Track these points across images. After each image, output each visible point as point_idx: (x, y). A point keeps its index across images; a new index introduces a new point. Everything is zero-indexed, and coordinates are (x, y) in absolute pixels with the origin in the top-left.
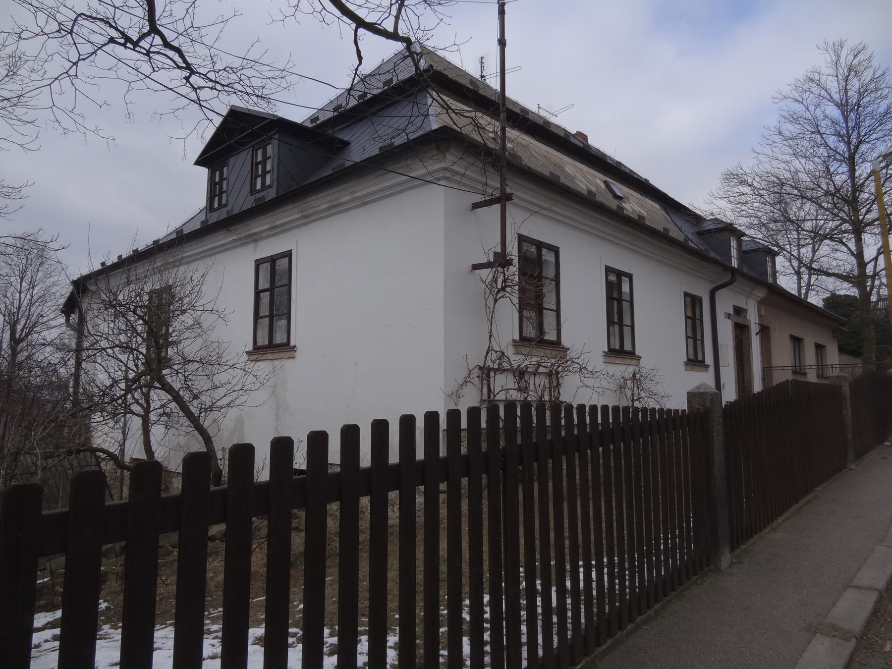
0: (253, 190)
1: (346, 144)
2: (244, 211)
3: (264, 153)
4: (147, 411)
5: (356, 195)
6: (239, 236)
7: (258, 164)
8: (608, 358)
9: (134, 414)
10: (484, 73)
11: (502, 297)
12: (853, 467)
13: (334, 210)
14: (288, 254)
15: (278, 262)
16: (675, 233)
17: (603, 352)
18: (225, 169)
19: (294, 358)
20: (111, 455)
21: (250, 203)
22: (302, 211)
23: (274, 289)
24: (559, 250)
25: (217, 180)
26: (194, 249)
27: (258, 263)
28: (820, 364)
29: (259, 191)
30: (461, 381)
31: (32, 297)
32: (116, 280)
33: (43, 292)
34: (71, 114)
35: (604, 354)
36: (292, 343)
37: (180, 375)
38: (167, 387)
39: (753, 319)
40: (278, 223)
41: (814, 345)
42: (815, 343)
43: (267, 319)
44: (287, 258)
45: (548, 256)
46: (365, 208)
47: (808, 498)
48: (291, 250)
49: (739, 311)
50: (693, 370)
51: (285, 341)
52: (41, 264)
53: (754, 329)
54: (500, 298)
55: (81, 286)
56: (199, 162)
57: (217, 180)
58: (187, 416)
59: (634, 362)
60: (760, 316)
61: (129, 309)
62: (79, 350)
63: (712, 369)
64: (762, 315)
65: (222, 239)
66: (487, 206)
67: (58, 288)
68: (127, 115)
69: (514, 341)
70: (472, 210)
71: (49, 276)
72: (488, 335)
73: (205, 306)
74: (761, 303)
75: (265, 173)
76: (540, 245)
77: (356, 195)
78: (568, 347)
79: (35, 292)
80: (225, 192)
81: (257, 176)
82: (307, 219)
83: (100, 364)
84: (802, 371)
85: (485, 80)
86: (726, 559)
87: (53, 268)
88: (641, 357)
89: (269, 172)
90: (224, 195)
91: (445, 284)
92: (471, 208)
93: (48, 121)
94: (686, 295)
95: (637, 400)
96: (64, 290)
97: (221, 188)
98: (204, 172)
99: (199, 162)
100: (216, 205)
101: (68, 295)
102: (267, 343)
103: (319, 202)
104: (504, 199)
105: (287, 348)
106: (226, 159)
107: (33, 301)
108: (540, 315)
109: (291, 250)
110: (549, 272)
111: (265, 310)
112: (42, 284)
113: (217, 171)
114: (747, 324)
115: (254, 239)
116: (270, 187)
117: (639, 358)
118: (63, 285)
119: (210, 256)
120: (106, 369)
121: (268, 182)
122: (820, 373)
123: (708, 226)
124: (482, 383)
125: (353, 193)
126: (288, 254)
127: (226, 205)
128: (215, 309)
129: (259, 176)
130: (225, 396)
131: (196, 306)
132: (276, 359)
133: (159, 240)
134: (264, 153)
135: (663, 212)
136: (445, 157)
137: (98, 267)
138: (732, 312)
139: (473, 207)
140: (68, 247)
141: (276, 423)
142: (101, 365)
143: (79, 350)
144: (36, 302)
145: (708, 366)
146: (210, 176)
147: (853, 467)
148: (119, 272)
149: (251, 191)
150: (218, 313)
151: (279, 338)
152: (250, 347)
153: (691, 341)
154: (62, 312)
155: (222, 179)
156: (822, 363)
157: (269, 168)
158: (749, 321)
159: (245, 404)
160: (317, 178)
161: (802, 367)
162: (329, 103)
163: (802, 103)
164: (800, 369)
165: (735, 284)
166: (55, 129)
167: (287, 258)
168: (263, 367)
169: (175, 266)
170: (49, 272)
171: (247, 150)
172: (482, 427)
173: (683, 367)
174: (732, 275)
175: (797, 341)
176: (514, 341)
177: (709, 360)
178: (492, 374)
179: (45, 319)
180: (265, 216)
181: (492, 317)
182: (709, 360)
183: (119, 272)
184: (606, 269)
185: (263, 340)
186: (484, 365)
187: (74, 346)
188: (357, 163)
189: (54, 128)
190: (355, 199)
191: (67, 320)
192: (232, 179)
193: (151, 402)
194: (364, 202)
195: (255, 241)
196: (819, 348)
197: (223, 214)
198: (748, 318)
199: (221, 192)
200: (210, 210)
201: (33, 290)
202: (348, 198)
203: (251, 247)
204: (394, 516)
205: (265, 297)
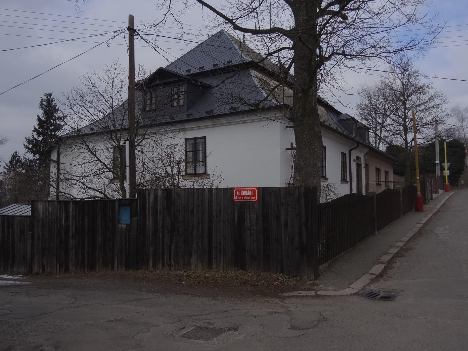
12: (402, 217)
13: (230, 124)
16: (340, 130)
22: (214, 122)
27: (186, 140)
28: (386, 181)
36: (208, 173)
39: (363, 161)
40: (200, 125)
41: (375, 168)
42: (356, 156)
47: (391, 224)
49: (358, 158)
51: (203, 172)
53: (363, 165)
59: (326, 181)
60: (365, 160)
63: (349, 183)
74: (366, 154)
82: (215, 125)
84: (380, 183)
85: (245, 42)
86: (376, 233)
94: (342, 153)
102: (194, 172)
115: (185, 130)
122: (386, 184)
123: (342, 117)
126: (205, 138)
135: (326, 112)
138: (356, 159)
147: (402, 217)
153: (343, 172)
156: (387, 181)
163: (388, 79)
164: (379, 183)
165: (359, 148)
175: (378, 170)
177: (348, 180)
182: (348, 180)
184: (376, 169)
186: (290, 182)
190: (241, 121)
194: (243, 123)
196: (386, 173)
198: (361, 161)
203: (182, 133)
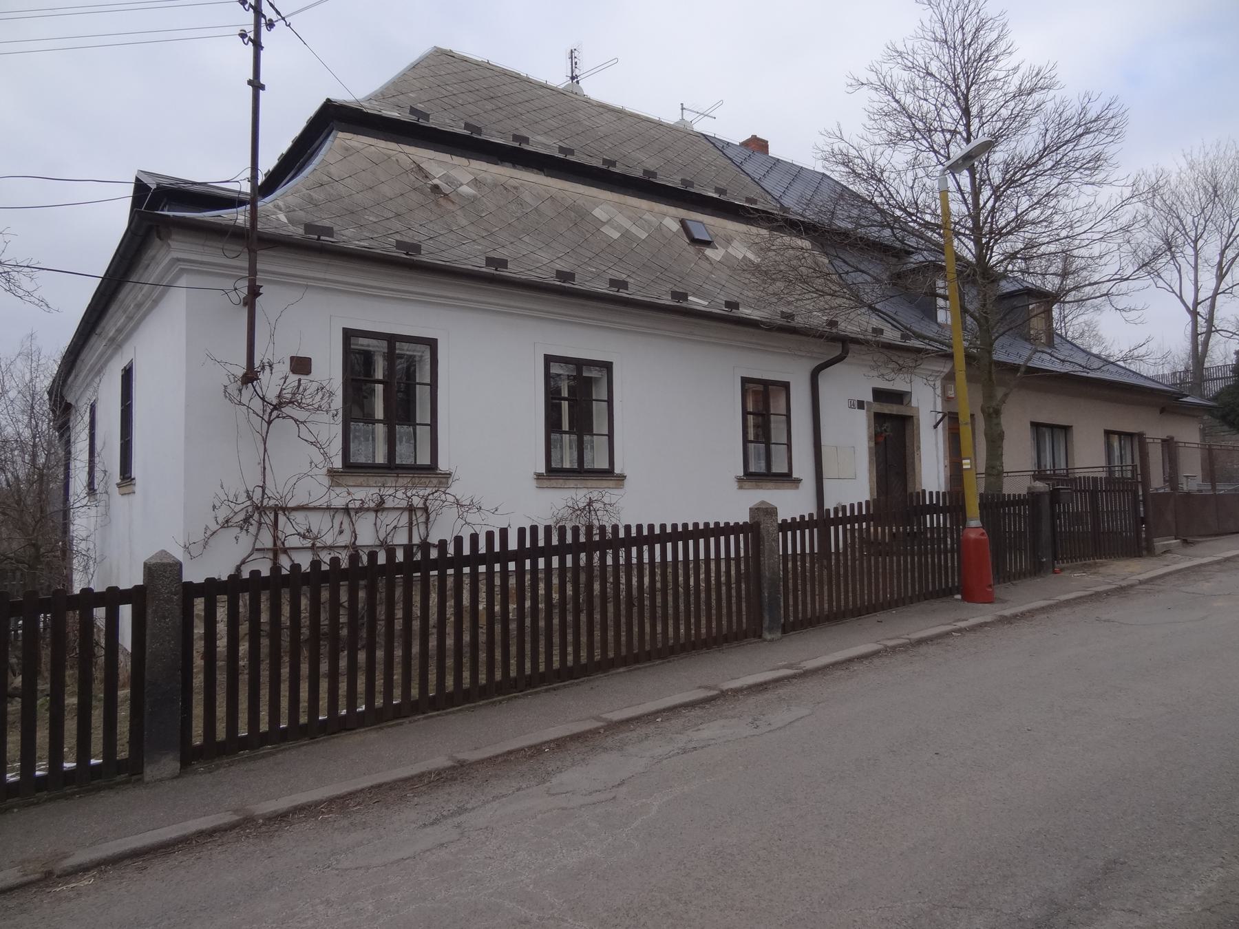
10: (577, 72)
11: (278, 417)
26: (92, 357)
45: (425, 353)
110: (423, 375)
114: (909, 414)
117: (622, 478)
145: (798, 481)
156: (1067, 466)
172: (608, 564)
174: (843, 347)
204: (466, 674)
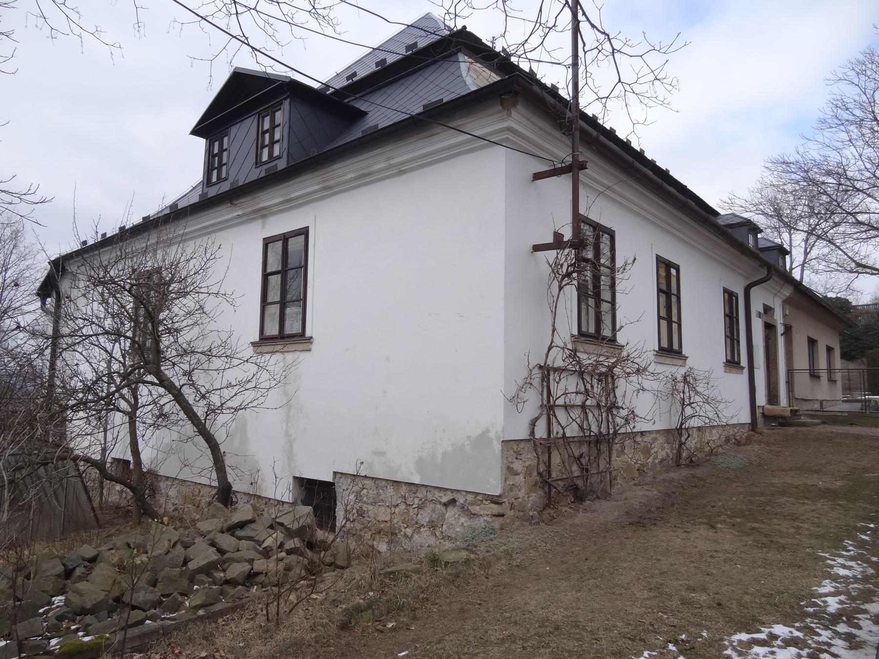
0: (258, 163)
1: (364, 114)
2: (261, 178)
3: (273, 120)
4: (135, 407)
5: (393, 162)
6: (246, 211)
7: (264, 133)
8: (658, 357)
9: (118, 410)
13: (365, 179)
14: (304, 232)
15: (291, 242)
17: (654, 350)
18: (226, 139)
19: (310, 350)
20: (94, 464)
21: (256, 174)
22: (324, 181)
23: (286, 271)
24: (614, 234)
25: (216, 151)
27: (267, 242)
28: (812, 368)
29: (266, 163)
30: (521, 383)
31: (5, 280)
32: (107, 256)
33: (16, 276)
34: (62, 7)
35: (655, 353)
36: (308, 334)
37: (176, 368)
38: (166, 383)
39: (778, 318)
40: (293, 195)
43: (278, 306)
44: (303, 236)
46: (401, 177)
48: (308, 227)
49: (768, 310)
50: (730, 372)
52: (15, 247)
53: (780, 329)
54: (566, 285)
55: (60, 266)
56: (196, 132)
57: (216, 151)
58: (190, 418)
60: (785, 316)
61: (124, 288)
62: (57, 336)
63: (746, 371)
64: (786, 315)
65: (225, 213)
66: (557, 175)
67: (32, 272)
68: (136, 26)
69: (572, 336)
70: (533, 181)
71: (23, 259)
72: (551, 328)
73: (210, 288)
74: (786, 302)
75: (273, 143)
76: (597, 227)
77: (393, 162)
78: (622, 344)
79: (7, 275)
80: (225, 164)
81: (263, 147)
82: (329, 191)
83: (81, 353)
84: (816, 374)
87: (27, 250)
88: (687, 357)
89: (278, 141)
90: (224, 168)
91: (506, 266)
92: (532, 179)
93: (29, 14)
95: (688, 405)
96: (40, 271)
97: (220, 160)
98: (201, 143)
99: (196, 132)
100: (214, 179)
101: (42, 280)
103: (346, 169)
104: (574, 169)
105: (301, 338)
106: (228, 128)
107: (6, 285)
108: (598, 305)
109: (308, 227)
111: (274, 295)
112: (16, 267)
113: (216, 141)
114: (774, 324)
115: (263, 214)
116: (279, 157)
118: (38, 269)
119: (209, 233)
120: (88, 358)
121: (276, 152)
124: (542, 385)
125: (388, 159)
126: (304, 232)
127: (226, 179)
128: (222, 292)
129: (267, 146)
130: (235, 395)
131: (201, 288)
132: (288, 352)
133: (149, 217)
134: (273, 120)
136: (510, 115)
137: (76, 247)
138: (762, 311)
139: (533, 177)
140: (50, 201)
141: (287, 425)
142: (82, 355)
143: (57, 336)
144: (8, 286)
145: (743, 368)
146: (208, 147)
148: (108, 250)
149: (256, 163)
150: (224, 297)
151: (293, 327)
152: (256, 338)
154: (38, 294)
155: (221, 150)
157: (277, 136)
158: (776, 320)
159: (262, 406)
160: (337, 145)
161: (815, 371)
162: (335, 76)
166: (39, 27)
167: (303, 236)
168: (275, 361)
169: (174, 244)
170: (24, 255)
171: (252, 118)
173: (723, 369)
175: (812, 342)
176: (572, 336)
177: (744, 362)
178: (551, 373)
179: (18, 304)
180: (278, 187)
181: (556, 307)
182: (744, 362)
183: (108, 250)
185: (272, 329)
186: (545, 364)
187: (50, 332)
188: (412, 117)
189: (37, 27)
190: (391, 167)
191: (44, 303)
192: (233, 151)
193: (139, 397)
195: (264, 216)
197: (225, 187)
199: (221, 165)
200: (207, 184)
201: (6, 273)
202: (382, 165)
203: (258, 224)
205: (275, 281)
